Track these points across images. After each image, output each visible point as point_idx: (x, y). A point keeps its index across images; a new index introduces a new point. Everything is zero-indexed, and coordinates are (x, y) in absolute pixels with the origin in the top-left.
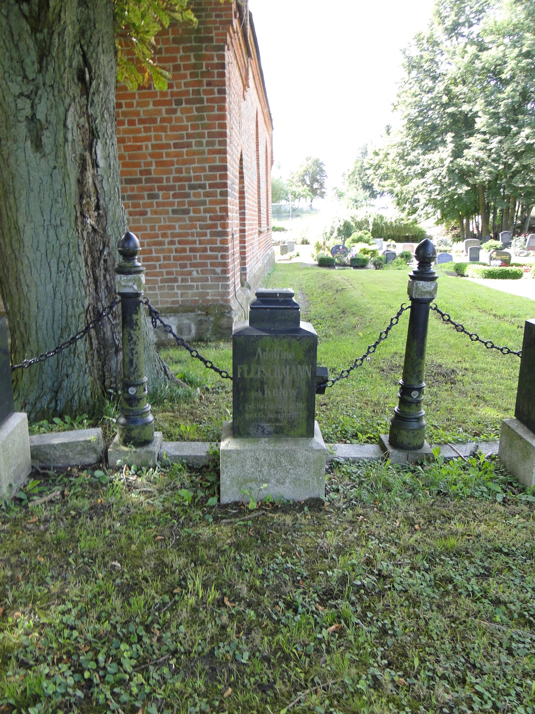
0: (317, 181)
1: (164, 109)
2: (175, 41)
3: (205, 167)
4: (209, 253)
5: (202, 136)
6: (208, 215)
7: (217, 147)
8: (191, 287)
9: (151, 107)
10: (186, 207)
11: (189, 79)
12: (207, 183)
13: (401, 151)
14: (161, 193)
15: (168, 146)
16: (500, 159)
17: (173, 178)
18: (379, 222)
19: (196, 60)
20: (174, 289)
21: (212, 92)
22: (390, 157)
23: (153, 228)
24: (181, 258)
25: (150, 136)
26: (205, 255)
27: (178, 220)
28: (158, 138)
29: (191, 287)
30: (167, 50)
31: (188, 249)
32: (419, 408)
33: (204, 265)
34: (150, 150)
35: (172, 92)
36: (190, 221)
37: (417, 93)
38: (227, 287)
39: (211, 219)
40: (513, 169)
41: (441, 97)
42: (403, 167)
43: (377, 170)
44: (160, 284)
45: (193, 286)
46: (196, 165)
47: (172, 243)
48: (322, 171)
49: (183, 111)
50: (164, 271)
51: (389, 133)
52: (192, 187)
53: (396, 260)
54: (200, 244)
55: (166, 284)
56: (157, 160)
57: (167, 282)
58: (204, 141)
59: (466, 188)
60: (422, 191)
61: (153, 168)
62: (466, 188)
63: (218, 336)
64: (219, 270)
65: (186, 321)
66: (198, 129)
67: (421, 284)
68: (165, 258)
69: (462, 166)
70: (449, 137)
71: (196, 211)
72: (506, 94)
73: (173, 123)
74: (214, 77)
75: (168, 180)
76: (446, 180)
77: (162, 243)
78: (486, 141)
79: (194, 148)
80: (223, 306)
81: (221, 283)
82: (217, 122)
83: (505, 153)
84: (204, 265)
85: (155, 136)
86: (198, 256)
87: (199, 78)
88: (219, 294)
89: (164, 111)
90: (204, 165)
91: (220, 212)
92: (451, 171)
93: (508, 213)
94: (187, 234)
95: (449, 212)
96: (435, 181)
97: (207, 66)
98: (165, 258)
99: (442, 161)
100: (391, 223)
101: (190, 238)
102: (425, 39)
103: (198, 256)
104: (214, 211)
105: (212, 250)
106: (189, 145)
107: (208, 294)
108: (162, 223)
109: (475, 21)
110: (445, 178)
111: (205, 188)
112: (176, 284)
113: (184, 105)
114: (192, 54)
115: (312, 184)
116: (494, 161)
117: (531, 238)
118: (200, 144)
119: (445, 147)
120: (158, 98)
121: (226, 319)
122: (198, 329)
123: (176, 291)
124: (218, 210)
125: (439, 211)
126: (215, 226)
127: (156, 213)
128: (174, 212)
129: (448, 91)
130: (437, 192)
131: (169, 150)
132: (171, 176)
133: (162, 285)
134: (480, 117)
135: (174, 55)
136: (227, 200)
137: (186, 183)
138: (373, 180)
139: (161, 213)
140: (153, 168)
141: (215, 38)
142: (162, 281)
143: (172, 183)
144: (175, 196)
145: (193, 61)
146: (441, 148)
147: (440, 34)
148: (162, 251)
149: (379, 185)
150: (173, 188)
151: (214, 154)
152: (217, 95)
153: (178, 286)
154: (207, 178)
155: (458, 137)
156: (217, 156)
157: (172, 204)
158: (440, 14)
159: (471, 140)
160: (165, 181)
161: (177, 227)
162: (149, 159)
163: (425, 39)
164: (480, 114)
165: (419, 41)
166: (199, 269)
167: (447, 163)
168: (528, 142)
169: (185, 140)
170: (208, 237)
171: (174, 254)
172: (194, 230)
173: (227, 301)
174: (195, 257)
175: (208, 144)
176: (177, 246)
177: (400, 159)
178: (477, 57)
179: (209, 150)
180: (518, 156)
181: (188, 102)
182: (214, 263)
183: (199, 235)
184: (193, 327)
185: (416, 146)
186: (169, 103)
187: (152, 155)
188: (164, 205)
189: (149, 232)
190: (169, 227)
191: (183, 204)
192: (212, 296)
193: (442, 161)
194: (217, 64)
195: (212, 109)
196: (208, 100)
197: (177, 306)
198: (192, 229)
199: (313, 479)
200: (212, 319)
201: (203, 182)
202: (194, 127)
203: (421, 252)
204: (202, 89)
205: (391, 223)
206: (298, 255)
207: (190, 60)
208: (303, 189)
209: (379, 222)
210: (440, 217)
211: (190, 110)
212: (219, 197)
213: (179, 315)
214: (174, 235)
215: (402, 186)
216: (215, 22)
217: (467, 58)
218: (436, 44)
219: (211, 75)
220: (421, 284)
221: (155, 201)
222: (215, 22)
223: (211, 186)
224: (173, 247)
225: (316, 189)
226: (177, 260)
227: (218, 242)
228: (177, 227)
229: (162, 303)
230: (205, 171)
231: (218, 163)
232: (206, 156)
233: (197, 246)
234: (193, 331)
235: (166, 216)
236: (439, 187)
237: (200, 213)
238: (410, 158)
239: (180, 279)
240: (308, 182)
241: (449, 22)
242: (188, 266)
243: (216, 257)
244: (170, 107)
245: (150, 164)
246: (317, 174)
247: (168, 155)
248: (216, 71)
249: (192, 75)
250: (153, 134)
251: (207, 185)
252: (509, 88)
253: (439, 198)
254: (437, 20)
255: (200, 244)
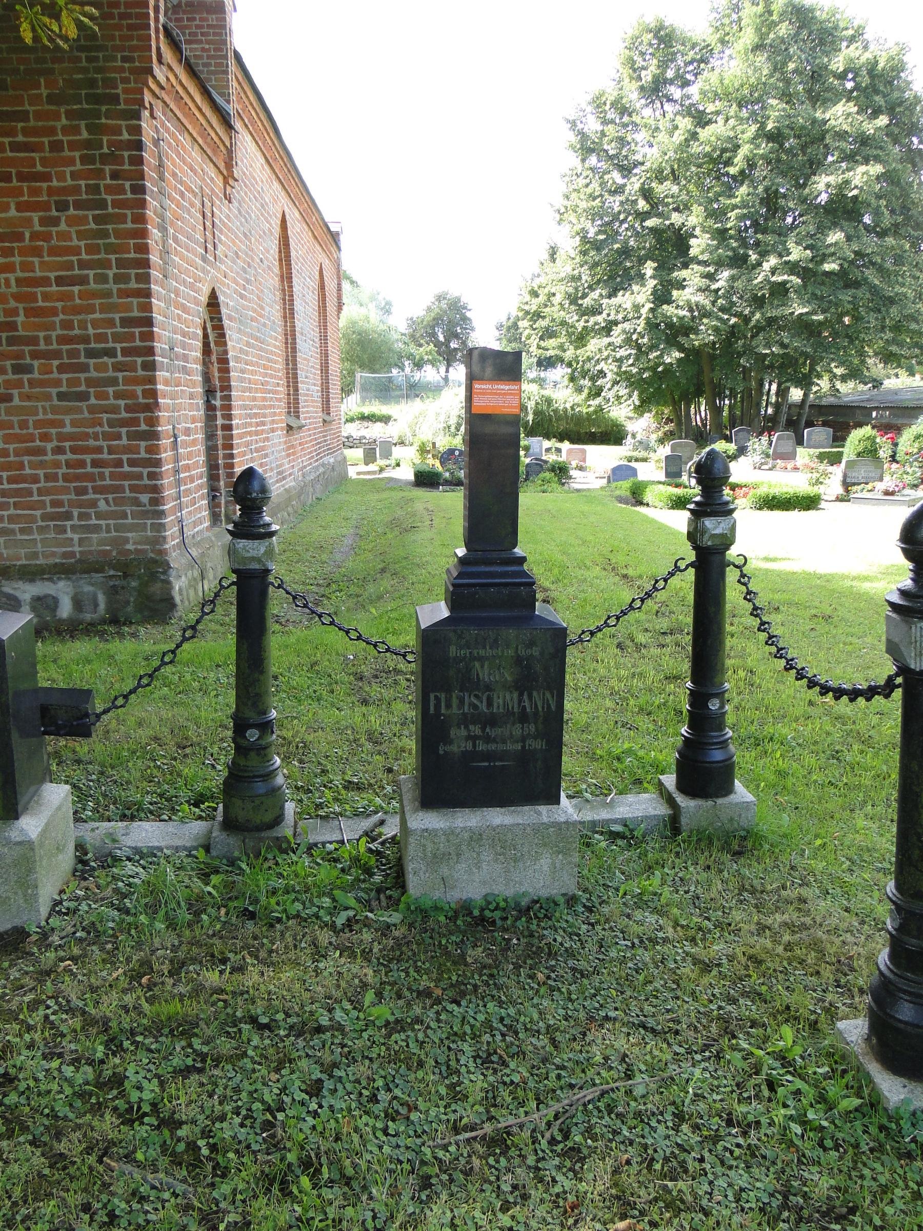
0: (456, 336)
1: (35, 217)
2: (51, 99)
3: (113, 320)
4: (126, 468)
5: (106, 264)
6: (122, 403)
7: (133, 285)
8: (96, 529)
9: (13, 212)
10: (83, 388)
11: (79, 166)
12: (118, 346)
13: (571, 290)
14: (36, 363)
15: (45, 282)
16: (731, 308)
17: (58, 337)
18: (545, 408)
19: (90, 133)
20: (65, 532)
21: (121, 190)
22: (557, 300)
23: (23, 425)
24: (77, 478)
25: (14, 263)
26: (121, 473)
27: (69, 411)
28: (26, 267)
29: (96, 529)
30: (38, 116)
31: (88, 461)
32: (268, 760)
33: (119, 489)
34: (14, 289)
35: (49, 188)
36: (89, 413)
37: (597, 194)
38: (161, 527)
39: (128, 409)
40: (753, 323)
41: (635, 202)
42: (576, 318)
43: (535, 321)
44: (40, 523)
45: (99, 526)
46: (97, 315)
47: (59, 450)
48: (465, 319)
49: (71, 221)
50: (47, 499)
51: (553, 259)
52: (91, 354)
53: (542, 475)
54: (110, 453)
55: (52, 523)
56: (27, 305)
57: (52, 520)
58: (111, 273)
59: (677, 355)
60: (606, 359)
61: (21, 319)
62: (677, 355)
63: (146, 614)
64: (144, 498)
65: (88, 589)
66: (99, 253)
67: (241, 545)
68: (48, 478)
69: (671, 317)
70: (649, 268)
71: (100, 396)
72: (738, 199)
73: (54, 242)
74: (123, 164)
75: (48, 340)
76: (645, 340)
77: (40, 451)
78: (711, 277)
79: (93, 286)
80: (155, 561)
81: (149, 522)
82: (132, 242)
83: (741, 298)
84: (120, 489)
85: (21, 263)
86: (107, 474)
87: (98, 166)
88: (147, 541)
89: (36, 220)
90: (111, 315)
91: (144, 397)
92: (652, 326)
93: (752, 399)
94: (86, 436)
95: (653, 395)
96: (628, 341)
97: (111, 144)
98: (48, 478)
99: (637, 307)
100: (565, 410)
101: (92, 443)
102: (608, 103)
103: (107, 474)
104: (133, 395)
105: (132, 463)
106: (83, 281)
107: (127, 541)
108: (41, 416)
109: (689, 77)
110: (643, 337)
111: (116, 356)
112: (69, 523)
113: (72, 211)
114: (83, 124)
115: (448, 341)
116: (722, 309)
117: (778, 439)
118: (103, 279)
119: (643, 285)
120: (26, 198)
121: (159, 585)
122: (109, 603)
123: (69, 534)
124: (140, 393)
125: (636, 393)
126: (135, 422)
127: (29, 398)
128: (61, 396)
129: (646, 193)
130: (631, 361)
131: (48, 289)
132: (54, 334)
133: (44, 524)
134: (696, 237)
135: (51, 123)
136: (155, 376)
137: (81, 347)
138: (529, 337)
139: (37, 399)
140: (21, 319)
141: (122, 97)
142: (45, 517)
143: (55, 346)
144: (61, 369)
145: (85, 135)
146: (635, 288)
147: (632, 95)
148: (42, 465)
149: (539, 347)
150: (57, 354)
151: (128, 296)
152: (129, 195)
153: (72, 526)
154: (117, 338)
155: (664, 268)
156: (135, 301)
157: (58, 383)
158: (634, 62)
159: (684, 273)
160: (42, 342)
161: (68, 422)
162: (13, 304)
163: (608, 103)
164: (697, 232)
165: (598, 107)
166: (110, 496)
167: (644, 311)
168: (774, 279)
169: (77, 272)
170: (124, 441)
171: (64, 470)
172: (98, 429)
173: (163, 552)
174: (102, 476)
175: (118, 279)
176: (69, 456)
177: (571, 304)
178: (694, 136)
179: (119, 290)
180: (758, 302)
181: (78, 205)
182: (137, 485)
183: (107, 436)
184: (101, 599)
185: (599, 282)
186: (45, 207)
187: (17, 297)
188: (42, 383)
189: (17, 431)
190: (53, 423)
191: (77, 382)
192: (134, 543)
193: (637, 307)
194: (129, 140)
195: (122, 219)
196: (116, 204)
197: (73, 560)
198: (94, 426)
199: (16, 893)
200: (134, 584)
201: (111, 345)
202: (91, 249)
203: (241, 488)
204: (102, 183)
205: (565, 410)
206: (398, 465)
207: (80, 134)
208: (427, 350)
209: (545, 408)
210: (637, 403)
211: (83, 220)
212: (140, 372)
213: (74, 577)
214: (61, 437)
215: (576, 348)
216: (122, 70)
217: (678, 137)
218: (624, 111)
219: (119, 160)
220: (241, 545)
221: (26, 377)
222: (122, 70)
223: (125, 352)
224: (62, 458)
225: (455, 349)
226: (70, 482)
227: (142, 450)
228: (68, 422)
229: (45, 556)
230: (114, 326)
231: (136, 314)
232: (115, 300)
233: (105, 456)
234: (102, 606)
235: (47, 404)
236: (634, 352)
237: (108, 399)
238: (587, 302)
239: (76, 514)
240: (441, 338)
241: (647, 77)
242: (90, 491)
243: (139, 477)
244: (48, 214)
245: (15, 312)
246: (458, 324)
247: (46, 297)
248: (126, 154)
249: (85, 159)
250: (17, 259)
251: (119, 350)
252: (743, 190)
253: (635, 370)
254: (626, 72)
255: (110, 453)
